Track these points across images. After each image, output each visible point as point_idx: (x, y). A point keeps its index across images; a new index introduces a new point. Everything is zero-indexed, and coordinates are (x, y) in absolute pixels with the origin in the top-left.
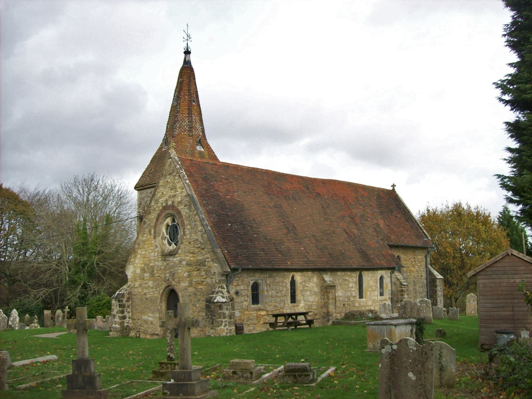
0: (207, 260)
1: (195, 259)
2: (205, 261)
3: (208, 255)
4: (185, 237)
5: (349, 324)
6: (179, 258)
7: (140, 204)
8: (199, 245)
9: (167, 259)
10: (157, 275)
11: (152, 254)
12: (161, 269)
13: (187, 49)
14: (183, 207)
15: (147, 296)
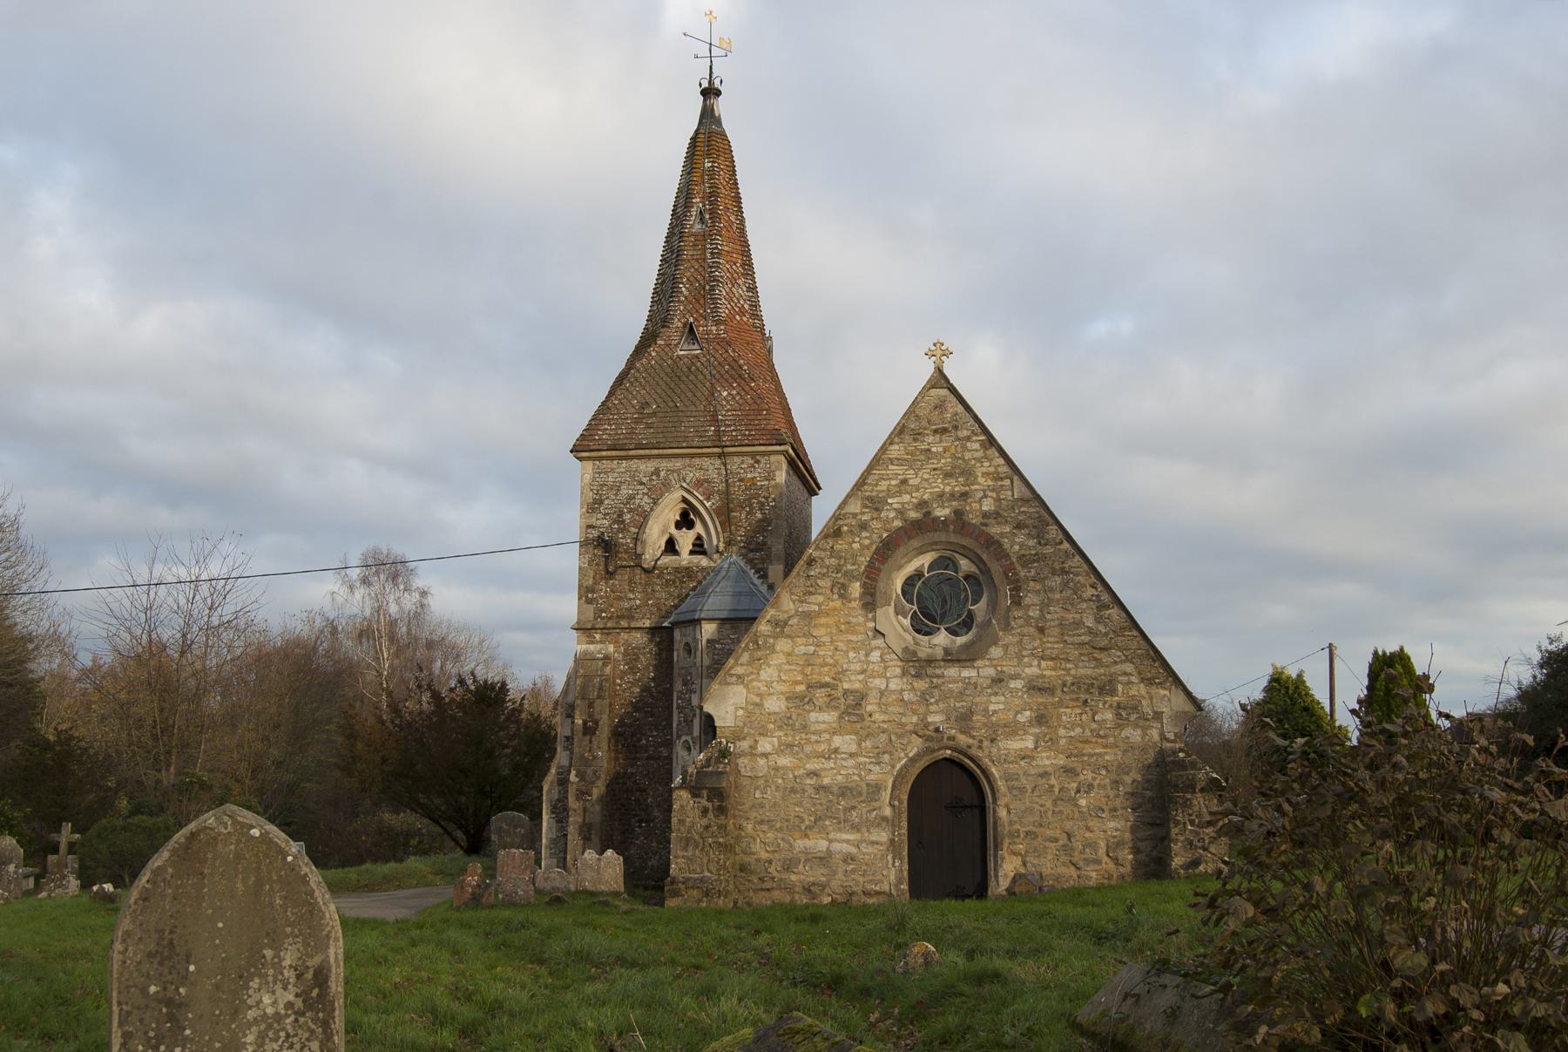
6: (991, 672)
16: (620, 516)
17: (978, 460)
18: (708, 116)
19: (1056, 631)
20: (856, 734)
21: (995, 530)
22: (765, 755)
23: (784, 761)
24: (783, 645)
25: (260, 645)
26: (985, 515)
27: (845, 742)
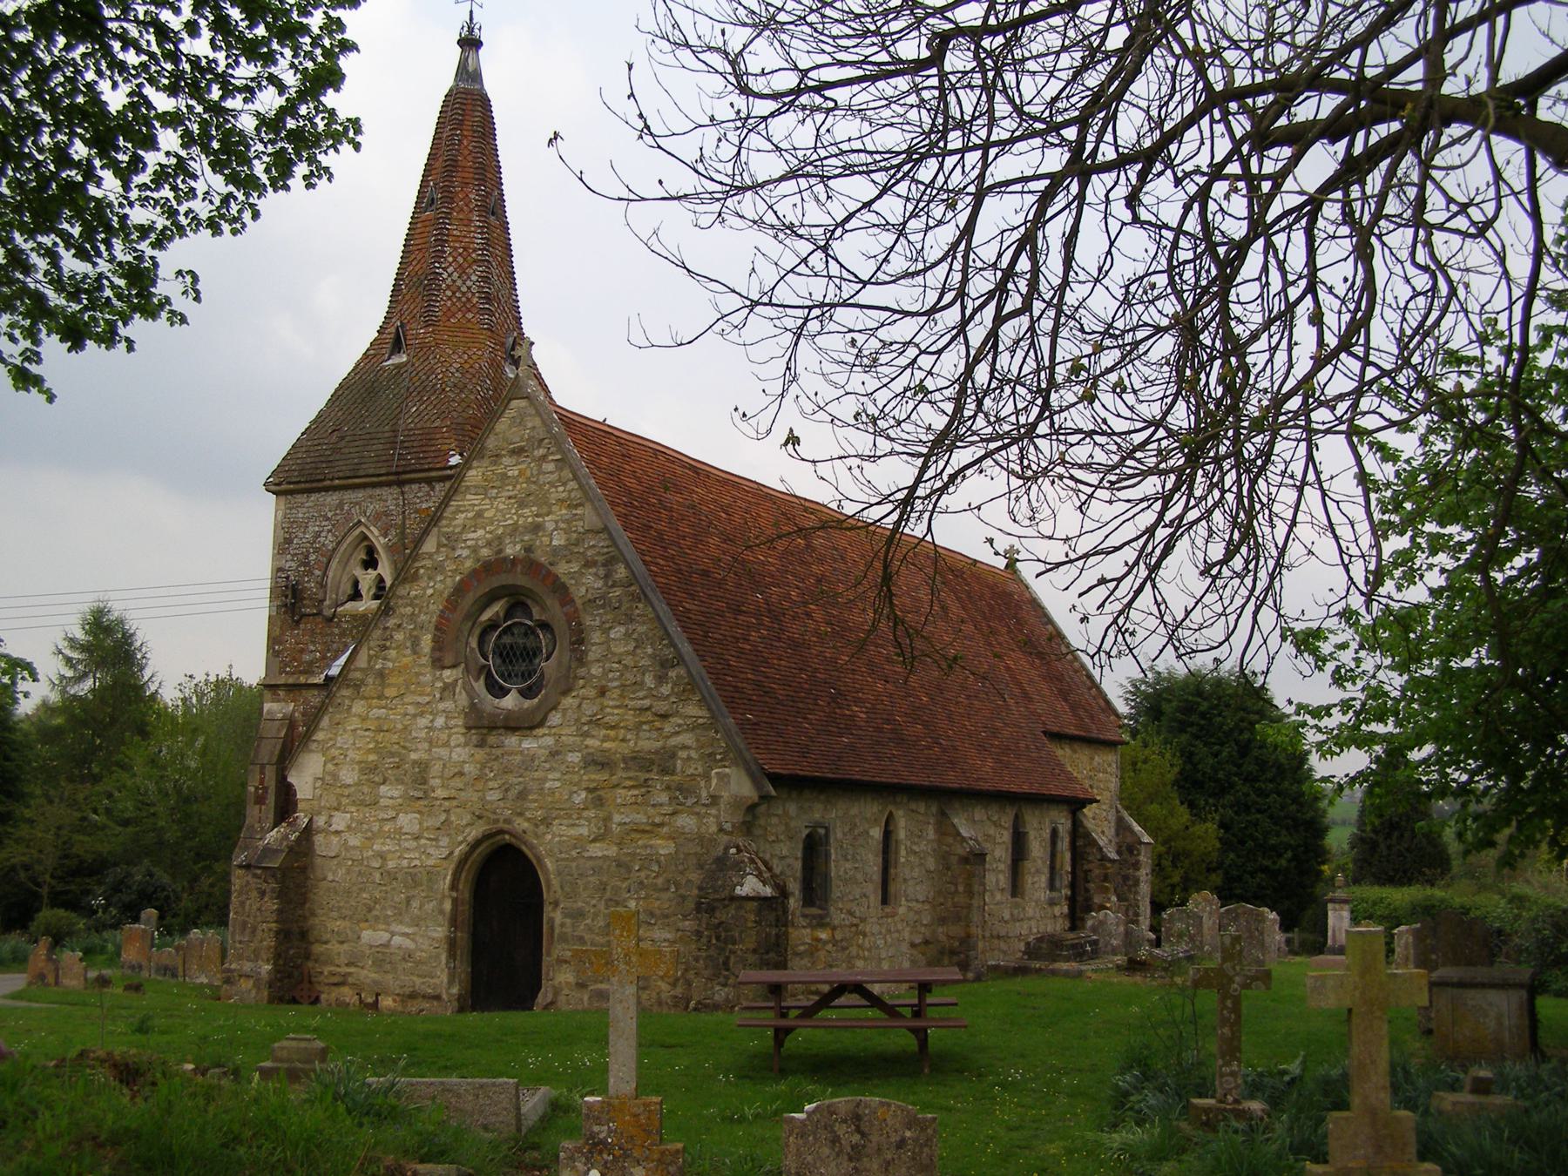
0: (683, 754)
1: (625, 749)
2: (673, 756)
3: (687, 738)
4: (582, 671)
5: (1054, 973)
6: (550, 741)
7: (289, 541)
8: (647, 702)
9: (492, 739)
10: (440, 793)
11: (423, 722)
12: (461, 774)
13: (471, 30)
14: (575, 567)
15: (391, 864)
16: (307, 557)
17: (552, 484)
18: (468, 75)
19: (616, 693)
20: (419, 812)
21: (562, 569)
22: (337, 832)
23: (354, 841)
24: (358, 707)
25: (220, 684)
26: (555, 551)
27: (408, 821)
